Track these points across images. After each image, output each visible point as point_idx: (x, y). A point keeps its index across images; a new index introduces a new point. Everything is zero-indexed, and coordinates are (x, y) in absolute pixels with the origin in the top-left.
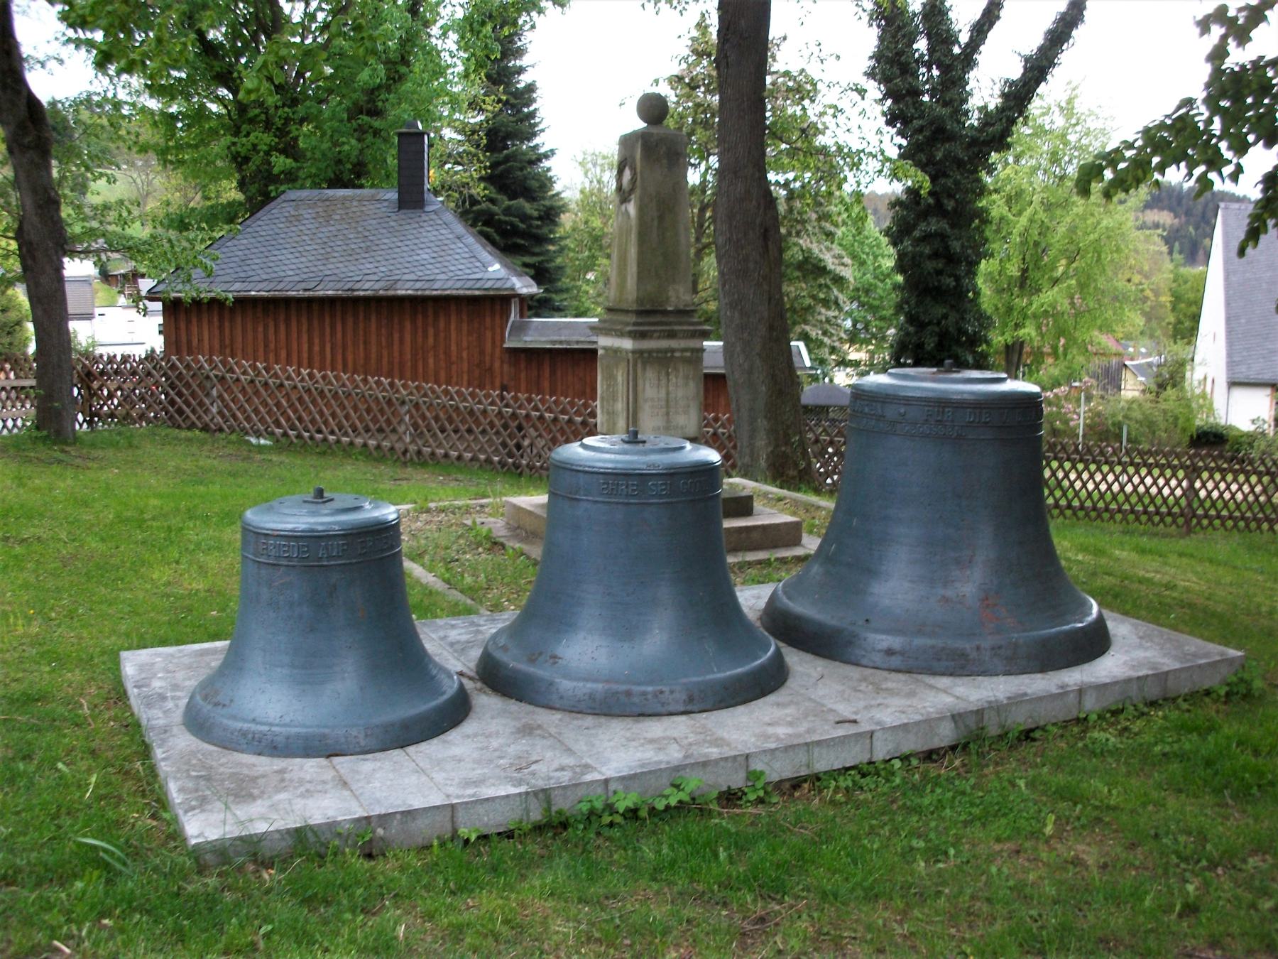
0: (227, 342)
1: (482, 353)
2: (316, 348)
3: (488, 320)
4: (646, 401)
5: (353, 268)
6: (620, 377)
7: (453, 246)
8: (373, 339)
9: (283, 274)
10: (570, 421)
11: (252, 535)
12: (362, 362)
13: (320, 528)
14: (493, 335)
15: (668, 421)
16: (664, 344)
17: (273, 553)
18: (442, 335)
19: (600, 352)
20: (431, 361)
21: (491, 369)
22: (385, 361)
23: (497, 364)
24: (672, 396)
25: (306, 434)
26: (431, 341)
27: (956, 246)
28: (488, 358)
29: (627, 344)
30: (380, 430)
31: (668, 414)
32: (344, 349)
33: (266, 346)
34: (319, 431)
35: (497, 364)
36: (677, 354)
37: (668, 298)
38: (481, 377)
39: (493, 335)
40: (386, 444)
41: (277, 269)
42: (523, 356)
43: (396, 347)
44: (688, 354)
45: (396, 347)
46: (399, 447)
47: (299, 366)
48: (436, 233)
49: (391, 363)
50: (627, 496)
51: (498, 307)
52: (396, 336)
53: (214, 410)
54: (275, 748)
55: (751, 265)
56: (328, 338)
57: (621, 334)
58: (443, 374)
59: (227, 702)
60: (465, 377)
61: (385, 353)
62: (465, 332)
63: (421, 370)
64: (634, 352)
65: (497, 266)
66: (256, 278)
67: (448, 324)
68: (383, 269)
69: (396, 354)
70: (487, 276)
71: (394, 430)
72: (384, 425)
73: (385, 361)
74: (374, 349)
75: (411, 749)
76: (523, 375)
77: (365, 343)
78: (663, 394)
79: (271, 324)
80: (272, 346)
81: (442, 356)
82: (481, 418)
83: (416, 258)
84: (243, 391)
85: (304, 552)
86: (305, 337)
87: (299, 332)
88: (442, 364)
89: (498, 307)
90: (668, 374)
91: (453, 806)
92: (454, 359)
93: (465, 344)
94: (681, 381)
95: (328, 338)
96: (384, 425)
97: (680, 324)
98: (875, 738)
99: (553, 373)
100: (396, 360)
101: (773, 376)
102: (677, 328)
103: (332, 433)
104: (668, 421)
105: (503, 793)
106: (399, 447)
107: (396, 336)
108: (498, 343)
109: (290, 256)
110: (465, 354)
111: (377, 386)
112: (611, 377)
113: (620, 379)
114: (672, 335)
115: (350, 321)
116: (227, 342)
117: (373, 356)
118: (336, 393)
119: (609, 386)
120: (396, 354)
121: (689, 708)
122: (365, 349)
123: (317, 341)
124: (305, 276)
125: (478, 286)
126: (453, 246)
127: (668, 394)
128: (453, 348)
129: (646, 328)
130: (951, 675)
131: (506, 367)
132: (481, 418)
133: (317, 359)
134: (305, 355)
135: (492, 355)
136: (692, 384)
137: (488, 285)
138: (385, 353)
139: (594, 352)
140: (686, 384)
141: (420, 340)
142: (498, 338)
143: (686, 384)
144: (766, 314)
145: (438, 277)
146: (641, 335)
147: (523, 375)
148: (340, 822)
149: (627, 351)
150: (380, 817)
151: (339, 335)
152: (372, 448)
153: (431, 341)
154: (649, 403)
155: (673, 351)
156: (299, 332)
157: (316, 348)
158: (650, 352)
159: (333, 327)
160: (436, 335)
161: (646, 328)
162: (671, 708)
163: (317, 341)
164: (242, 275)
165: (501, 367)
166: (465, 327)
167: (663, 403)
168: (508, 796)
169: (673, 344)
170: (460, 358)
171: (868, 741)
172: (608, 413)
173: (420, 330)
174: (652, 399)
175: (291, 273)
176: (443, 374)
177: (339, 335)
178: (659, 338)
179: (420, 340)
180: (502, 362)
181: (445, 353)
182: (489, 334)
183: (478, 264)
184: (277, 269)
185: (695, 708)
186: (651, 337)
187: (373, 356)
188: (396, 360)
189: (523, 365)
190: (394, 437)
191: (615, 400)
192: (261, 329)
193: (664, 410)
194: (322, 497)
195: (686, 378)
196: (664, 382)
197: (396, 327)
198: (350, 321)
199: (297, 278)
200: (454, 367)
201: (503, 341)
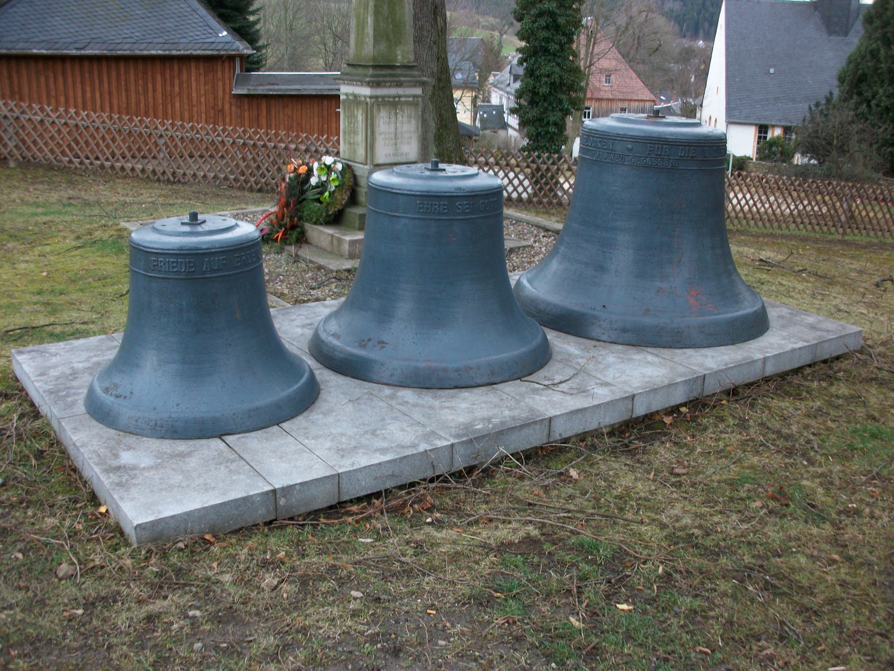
0: (16, 89)
1: (216, 98)
2: (89, 95)
3: (220, 74)
4: (380, 134)
5: (113, 33)
6: (360, 117)
7: (191, 17)
8: (132, 88)
9: (57, 36)
10: (286, 148)
11: (139, 253)
12: (124, 105)
13: (204, 247)
14: (224, 84)
15: (396, 149)
16: (393, 91)
17: (163, 269)
18: (185, 85)
19: (342, 97)
20: (177, 105)
21: (222, 110)
22: (142, 105)
23: (227, 107)
24: (399, 130)
25: (87, 161)
26: (177, 89)
27: (561, 21)
28: (220, 102)
29: (365, 91)
30: (133, 157)
31: (396, 144)
32: (110, 93)
33: (48, 93)
34: (97, 158)
35: (227, 107)
36: (403, 99)
37: (396, 56)
38: (216, 115)
39: (224, 84)
40: (150, 167)
41: (52, 33)
42: (246, 100)
43: (150, 95)
44: (411, 99)
45: (150, 95)
46: (160, 170)
47: (111, 110)
48: (177, 7)
49: (147, 106)
50: (439, 214)
51: (227, 64)
52: (150, 86)
53: (11, 145)
54: (176, 432)
55: (425, 33)
56: (97, 86)
57: (362, 83)
58: (186, 115)
59: (128, 394)
60: (204, 116)
61: (142, 98)
62: (202, 83)
63: (170, 111)
64: (371, 97)
65: (225, 33)
66: (36, 39)
67: (189, 76)
68: (138, 34)
69: (151, 100)
70: (218, 40)
71: (154, 157)
72: (147, 153)
73: (142, 105)
74: (133, 96)
75: (285, 425)
76: (246, 114)
77: (127, 91)
78: (392, 129)
79: (51, 75)
80: (53, 93)
81: (186, 101)
82: (220, 147)
83: (163, 26)
84: (35, 129)
85: (191, 267)
86: (79, 86)
87: (74, 82)
88: (186, 107)
89: (227, 64)
90: (396, 114)
91: (339, 475)
92: (194, 103)
93: (203, 92)
94: (405, 119)
95: (97, 86)
96: (147, 153)
97: (405, 76)
98: (635, 400)
99: (268, 112)
100: (151, 104)
101: (440, 115)
102: (403, 79)
103: (107, 159)
104: (396, 149)
105: (376, 461)
106: (160, 170)
107: (150, 86)
108: (228, 90)
109: (62, 22)
110: (203, 99)
111: (136, 124)
112: (352, 117)
113: (360, 118)
114: (399, 85)
115: (114, 74)
116: (16, 89)
117: (133, 101)
118: (109, 129)
119: (350, 123)
120: (151, 100)
121: (493, 380)
122: (127, 96)
123: (88, 89)
124: (75, 39)
125: (211, 47)
126: (191, 17)
127: (396, 129)
128: (194, 95)
129: (381, 79)
130: (670, 347)
131: (233, 108)
132: (220, 147)
133: (89, 103)
134: (80, 100)
135: (223, 99)
136: (413, 122)
137: (220, 47)
138: (142, 98)
139: (338, 96)
140: (409, 122)
141: (168, 89)
142: (227, 87)
143: (409, 122)
144: (435, 70)
145: (181, 41)
146: (376, 84)
147: (246, 114)
148: (252, 496)
149: (365, 97)
150: (283, 489)
151: (106, 85)
152: (118, 169)
153: (177, 89)
154: (383, 136)
155: (400, 97)
156: (74, 82)
157: (89, 95)
158: (383, 97)
159: (118, 75)
160: (180, 85)
161: (381, 79)
162: (479, 381)
163: (88, 89)
164: (25, 36)
165: (230, 108)
166: (202, 78)
167: (393, 136)
168: (380, 464)
169: (400, 91)
170: (200, 102)
171: (631, 403)
172: (350, 144)
173: (168, 81)
174: (385, 133)
175: (64, 36)
176: (186, 115)
177: (106, 85)
178: (390, 86)
179: (168, 89)
180: (231, 105)
181: (188, 98)
182: (220, 84)
183: (210, 31)
184: (52, 33)
185: (498, 379)
186: (384, 86)
187: (133, 101)
188: (151, 104)
189: (246, 107)
190: (155, 162)
191: (355, 133)
192: (43, 79)
193: (394, 141)
194: (197, 219)
195: (410, 116)
196: (393, 119)
197: (150, 78)
198: (114, 74)
199: (70, 40)
200: (195, 109)
201: (231, 90)
